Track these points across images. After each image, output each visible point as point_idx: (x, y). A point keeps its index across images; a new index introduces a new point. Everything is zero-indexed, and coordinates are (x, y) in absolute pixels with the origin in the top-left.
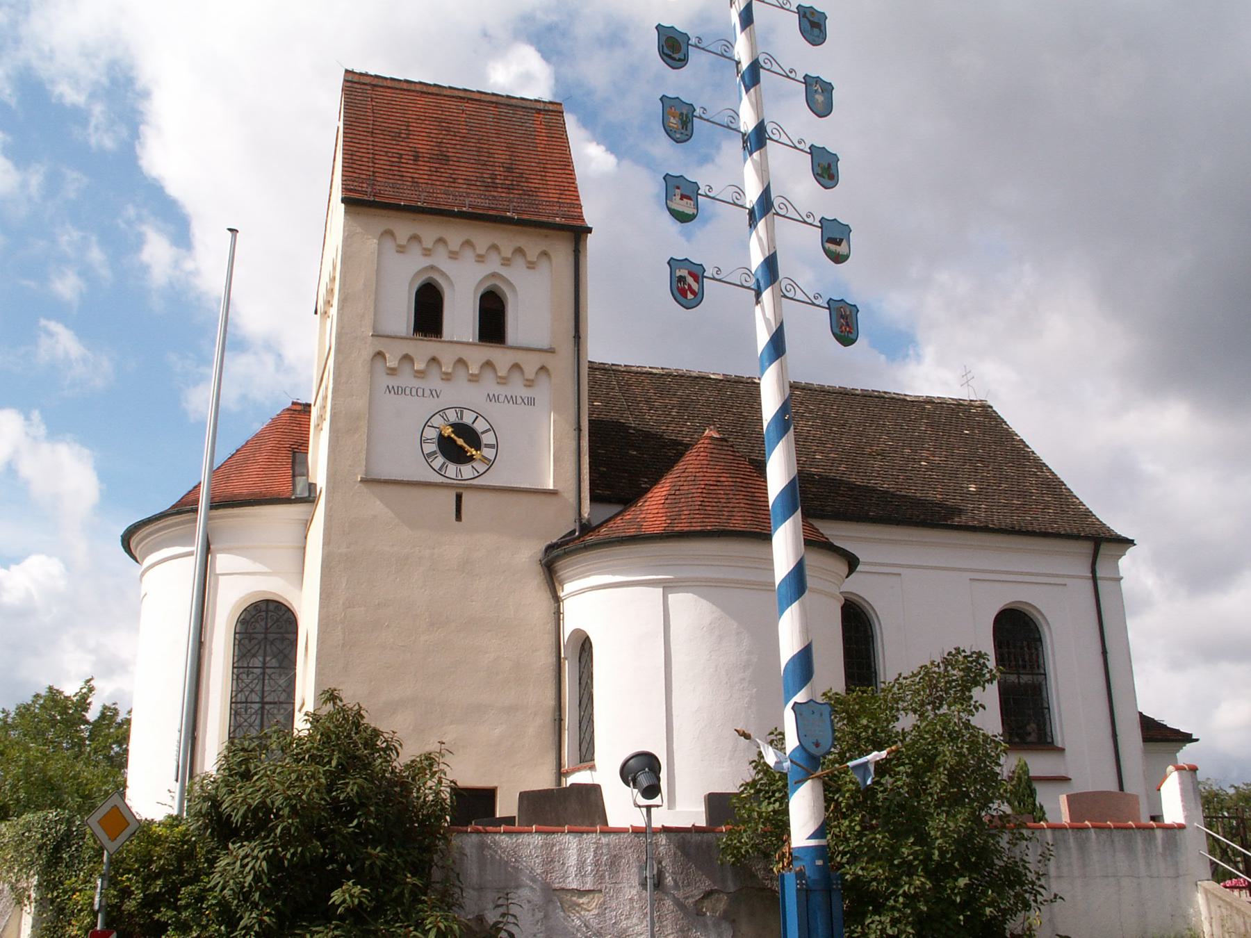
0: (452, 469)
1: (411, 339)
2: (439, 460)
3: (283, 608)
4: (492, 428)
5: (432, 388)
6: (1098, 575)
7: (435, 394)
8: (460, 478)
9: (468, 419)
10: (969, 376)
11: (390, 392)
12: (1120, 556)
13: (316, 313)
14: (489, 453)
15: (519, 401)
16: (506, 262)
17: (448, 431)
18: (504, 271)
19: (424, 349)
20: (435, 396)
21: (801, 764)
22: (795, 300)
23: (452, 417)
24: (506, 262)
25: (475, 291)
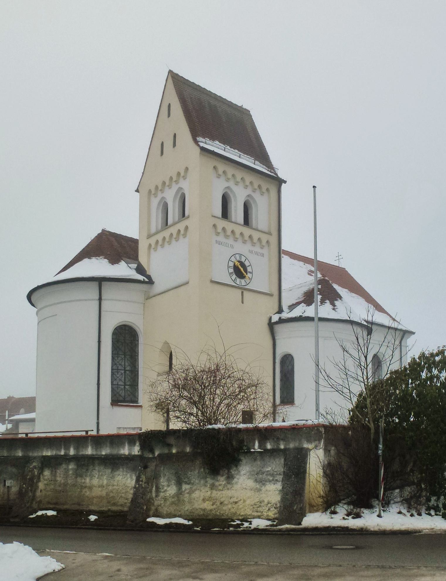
0: (238, 280)
1: (243, 226)
2: (234, 276)
3: (114, 367)
4: (228, 267)
5: (231, 244)
6: (402, 344)
7: (232, 247)
8: (241, 285)
9: (243, 259)
10: (340, 257)
11: (217, 243)
12: (408, 338)
13: (225, 214)
14: (249, 275)
15: (259, 254)
16: (254, 191)
17: (237, 264)
18: (253, 195)
19: (222, 224)
20: (232, 248)
21: (321, 458)
22: (348, 382)
23: (238, 257)
24: (254, 191)
25: (224, 189)
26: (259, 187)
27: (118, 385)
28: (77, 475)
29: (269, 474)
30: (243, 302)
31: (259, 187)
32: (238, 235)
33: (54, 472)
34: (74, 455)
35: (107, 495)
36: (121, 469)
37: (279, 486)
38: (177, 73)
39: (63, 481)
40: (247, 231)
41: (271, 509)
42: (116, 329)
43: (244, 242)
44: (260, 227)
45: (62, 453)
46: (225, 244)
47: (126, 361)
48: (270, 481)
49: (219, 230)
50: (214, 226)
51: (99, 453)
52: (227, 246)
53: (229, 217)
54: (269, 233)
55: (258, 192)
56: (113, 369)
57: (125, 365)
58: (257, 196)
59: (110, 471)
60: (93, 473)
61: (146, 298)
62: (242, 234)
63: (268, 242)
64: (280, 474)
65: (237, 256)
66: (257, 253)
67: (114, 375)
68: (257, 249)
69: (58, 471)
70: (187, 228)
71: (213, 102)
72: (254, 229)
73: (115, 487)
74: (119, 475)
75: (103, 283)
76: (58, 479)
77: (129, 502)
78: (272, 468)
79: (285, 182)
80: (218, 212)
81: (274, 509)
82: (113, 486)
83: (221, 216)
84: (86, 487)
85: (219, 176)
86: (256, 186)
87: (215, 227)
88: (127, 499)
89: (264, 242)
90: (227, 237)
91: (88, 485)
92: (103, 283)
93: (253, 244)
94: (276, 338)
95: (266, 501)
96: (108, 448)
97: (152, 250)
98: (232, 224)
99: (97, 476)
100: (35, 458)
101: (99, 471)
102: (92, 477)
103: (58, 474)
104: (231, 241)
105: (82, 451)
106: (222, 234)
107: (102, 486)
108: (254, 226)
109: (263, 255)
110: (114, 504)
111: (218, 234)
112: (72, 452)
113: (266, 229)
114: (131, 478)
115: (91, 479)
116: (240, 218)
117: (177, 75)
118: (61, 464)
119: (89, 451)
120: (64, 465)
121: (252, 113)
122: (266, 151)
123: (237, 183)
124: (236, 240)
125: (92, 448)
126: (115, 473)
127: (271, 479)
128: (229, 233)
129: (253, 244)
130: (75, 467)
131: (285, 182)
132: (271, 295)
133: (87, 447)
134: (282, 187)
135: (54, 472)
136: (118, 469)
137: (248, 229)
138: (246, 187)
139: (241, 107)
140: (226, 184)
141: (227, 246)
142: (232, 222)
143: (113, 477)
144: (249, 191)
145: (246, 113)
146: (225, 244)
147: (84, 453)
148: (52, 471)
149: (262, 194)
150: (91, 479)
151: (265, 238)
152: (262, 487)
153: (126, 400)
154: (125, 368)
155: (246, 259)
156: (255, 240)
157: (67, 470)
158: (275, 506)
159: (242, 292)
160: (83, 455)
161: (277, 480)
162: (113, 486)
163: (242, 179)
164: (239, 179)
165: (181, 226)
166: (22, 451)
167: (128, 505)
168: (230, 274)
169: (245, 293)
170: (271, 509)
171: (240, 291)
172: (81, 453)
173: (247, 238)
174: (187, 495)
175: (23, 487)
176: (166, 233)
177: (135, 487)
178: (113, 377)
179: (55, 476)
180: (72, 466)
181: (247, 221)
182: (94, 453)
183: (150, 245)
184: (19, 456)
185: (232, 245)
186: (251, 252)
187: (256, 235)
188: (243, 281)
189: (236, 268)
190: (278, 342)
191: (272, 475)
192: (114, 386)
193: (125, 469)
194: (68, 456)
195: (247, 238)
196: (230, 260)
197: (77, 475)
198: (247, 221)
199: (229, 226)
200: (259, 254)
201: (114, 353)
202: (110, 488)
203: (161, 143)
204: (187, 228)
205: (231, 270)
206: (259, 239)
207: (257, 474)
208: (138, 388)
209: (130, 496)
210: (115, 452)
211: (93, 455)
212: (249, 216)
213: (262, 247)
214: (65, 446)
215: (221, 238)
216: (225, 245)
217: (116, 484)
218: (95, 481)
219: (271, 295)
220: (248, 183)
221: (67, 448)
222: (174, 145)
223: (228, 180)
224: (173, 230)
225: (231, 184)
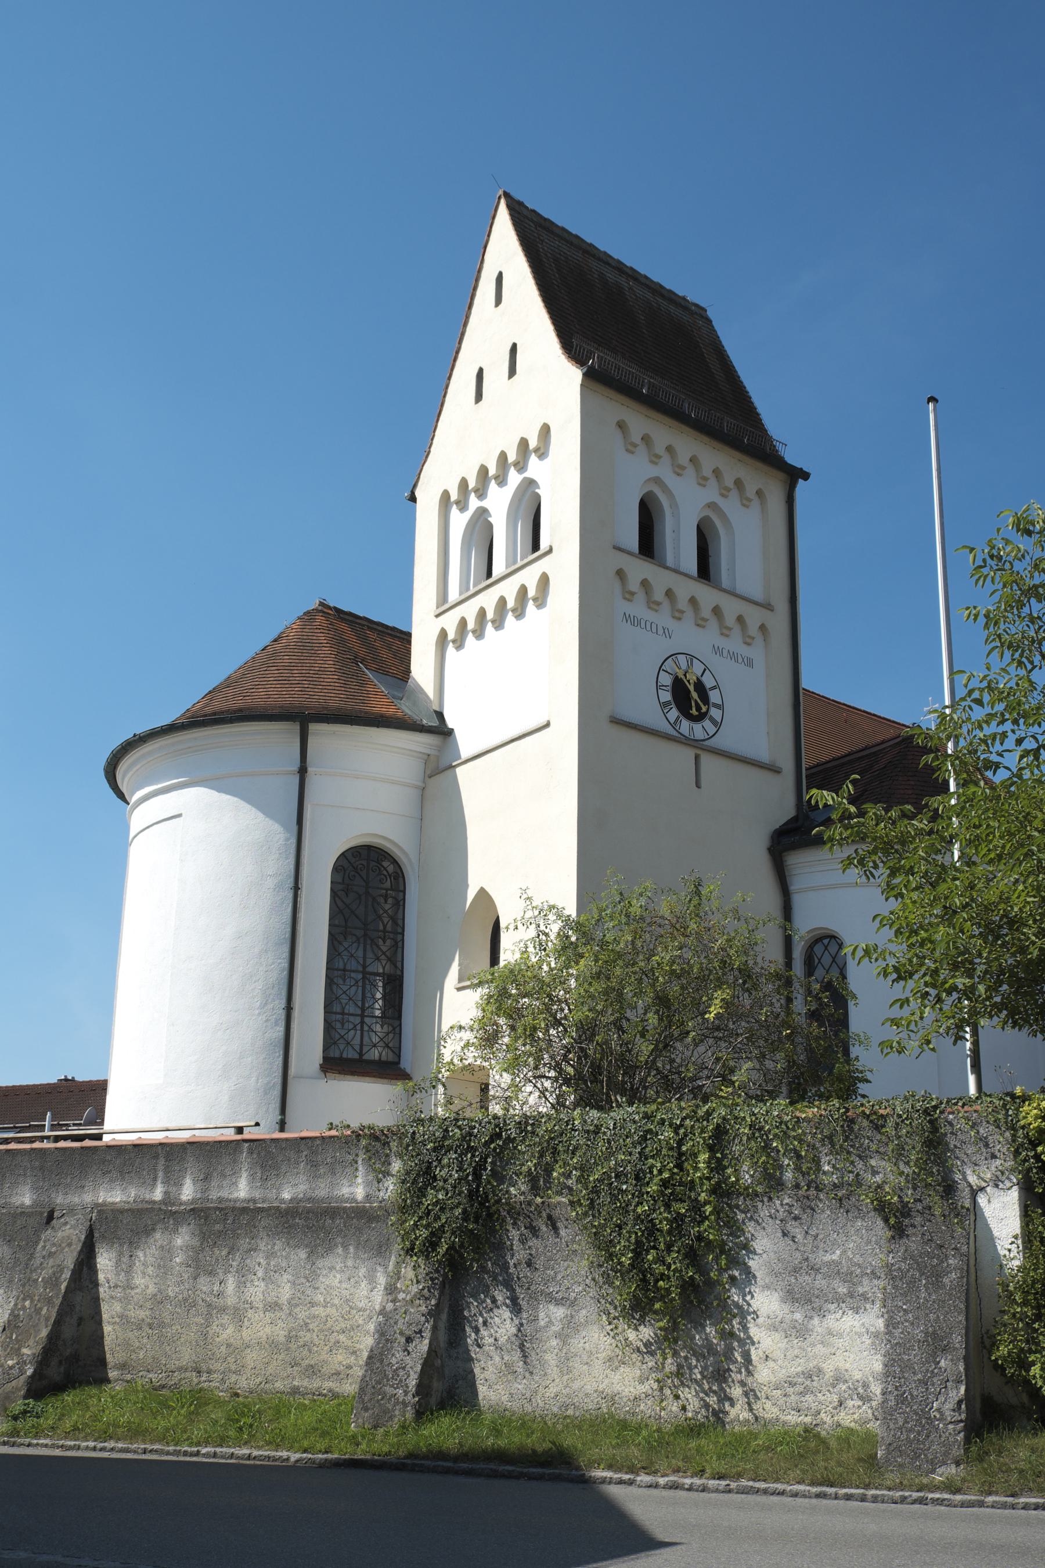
2: (674, 713)
7: (667, 633)
15: (740, 660)
16: (724, 492)
18: (721, 502)
19: (639, 569)
26: (739, 483)
27: (343, 1013)
28: (199, 1266)
29: (835, 1271)
30: (698, 785)
31: (739, 483)
32: (683, 603)
33: (125, 1259)
34: (194, 1201)
35: (289, 1338)
36: (340, 1250)
37: (874, 1319)
38: (521, 200)
39: (152, 1289)
40: (706, 595)
41: (850, 1403)
42: (343, 855)
43: (701, 623)
44: (741, 588)
45: (158, 1194)
46: (648, 625)
47: (368, 947)
48: (839, 1300)
49: (634, 585)
50: (620, 574)
51: (272, 1194)
52: (654, 630)
53: (656, 553)
54: (768, 607)
55: (734, 494)
56: (334, 969)
57: (365, 958)
58: (731, 506)
59: (303, 1254)
60: (248, 1261)
61: (428, 772)
62: (693, 601)
63: (763, 628)
64: (874, 1275)
65: (682, 659)
66: (733, 656)
67: (335, 987)
68: (734, 643)
69: (141, 1254)
70: (544, 581)
71: (611, 276)
72: (725, 591)
73: (319, 1311)
74: (332, 1268)
75: (313, 727)
76: (139, 1281)
77: (361, 1363)
78: (844, 1252)
79: (806, 476)
80: (632, 539)
81: (860, 1403)
82: (313, 1304)
83: (636, 550)
84: (223, 1310)
85: (631, 448)
86: (729, 482)
87: (621, 579)
88: (354, 1353)
89: (753, 629)
90: (652, 604)
91: (231, 1301)
92: (313, 727)
93: (725, 631)
94: (792, 888)
95: (829, 1375)
96: (302, 1178)
97: (451, 649)
98: (667, 572)
99: (260, 1273)
100: (72, 1210)
101: (270, 1255)
102: (244, 1274)
103: (138, 1266)
104: (663, 618)
105: (220, 1187)
106: (641, 596)
107: (273, 1306)
108: (725, 583)
109: (750, 663)
110: (312, 1371)
111: (629, 596)
112: (188, 1191)
113: (758, 594)
114: (372, 1280)
115: (241, 1285)
116: (690, 562)
117: (521, 204)
118: (149, 1231)
119: (242, 1189)
120: (158, 1235)
121: (710, 314)
122: (752, 403)
123: (679, 470)
124: (678, 615)
125: (252, 1177)
126: (320, 1263)
127: (843, 1290)
128: (659, 595)
129: (725, 631)
130: (195, 1242)
131: (806, 476)
132: (773, 769)
133: (236, 1174)
134: (797, 489)
135: (125, 1259)
136: (330, 1249)
137: (709, 588)
138: (702, 481)
139: (684, 298)
140: (653, 471)
141: (654, 630)
142: (667, 568)
143: (312, 1277)
144: (711, 493)
145: (699, 314)
146: (648, 625)
147: (224, 1194)
148: (121, 1254)
149: (745, 502)
150: (241, 1285)
151: (754, 617)
152: (811, 1318)
153: (365, 1057)
154: (364, 966)
155: (705, 670)
156: (730, 620)
157: (167, 1252)
158: (861, 1390)
159: (697, 758)
160: (220, 1200)
161: (864, 1297)
162: (313, 1304)
163: (691, 460)
164: (683, 459)
165: (529, 577)
166: (35, 1189)
167: (359, 1372)
168: (664, 705)
169: (706, 759)
170: (850, 1403)
171: (689, 753)
172: (214, 1195)
173: (706, 612)
174: (554, 1342)
175: (24, 1308)
176: (488, 600)
177: (382, 1312)
178: (332, 990)
179: (129, 1271)
180: (183, 1238)
181: (705, 570)
182: (257, 1194)
183: (443, 633)
184: (22, 1205)
185: (666, 631)
186: (717, 651)
187: (732, 608)
188: (697, 727)
189: (679, 689)
190: (797, 900)
191: (848, 1278)
192: (333, 1017)
193: (352, 1249)
194: (173, 1204)
195: (706, 612)
196: (663, 667)
197: (199, 1266)
198: (705, 570)
199: (661, 579)
200: (740, 660)
201: (337, 922)
202: (302, 1313)
203: (476, 371)
204: (544, 581)
205: (667, 696)
206: (740, 619)
207: (796, 1270)
208: (403, 940)
209: (367, 1342)
210: (322, 1191)
211: (254, 1200)
212: (711, 559)
213: (748, 641)
214: (167, 1171)
215: (638, 608)
216: (648, 628)
217: (322, 1300)
218: (256, 1291)
219: (773, 769)
220: (707, 471)
221: (174, 1181)
222: (512, 372)
223: (655, 459)
224: (508, 589)
225: (664, 471)
